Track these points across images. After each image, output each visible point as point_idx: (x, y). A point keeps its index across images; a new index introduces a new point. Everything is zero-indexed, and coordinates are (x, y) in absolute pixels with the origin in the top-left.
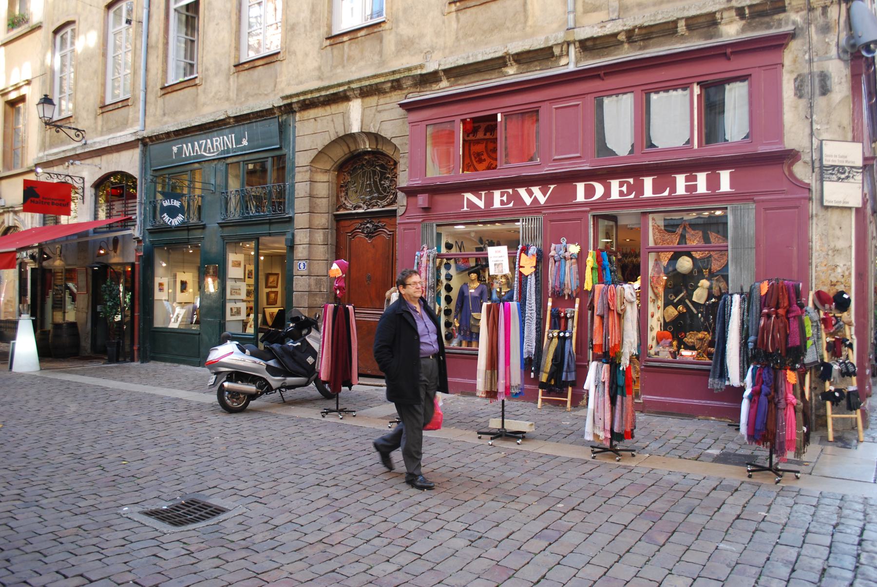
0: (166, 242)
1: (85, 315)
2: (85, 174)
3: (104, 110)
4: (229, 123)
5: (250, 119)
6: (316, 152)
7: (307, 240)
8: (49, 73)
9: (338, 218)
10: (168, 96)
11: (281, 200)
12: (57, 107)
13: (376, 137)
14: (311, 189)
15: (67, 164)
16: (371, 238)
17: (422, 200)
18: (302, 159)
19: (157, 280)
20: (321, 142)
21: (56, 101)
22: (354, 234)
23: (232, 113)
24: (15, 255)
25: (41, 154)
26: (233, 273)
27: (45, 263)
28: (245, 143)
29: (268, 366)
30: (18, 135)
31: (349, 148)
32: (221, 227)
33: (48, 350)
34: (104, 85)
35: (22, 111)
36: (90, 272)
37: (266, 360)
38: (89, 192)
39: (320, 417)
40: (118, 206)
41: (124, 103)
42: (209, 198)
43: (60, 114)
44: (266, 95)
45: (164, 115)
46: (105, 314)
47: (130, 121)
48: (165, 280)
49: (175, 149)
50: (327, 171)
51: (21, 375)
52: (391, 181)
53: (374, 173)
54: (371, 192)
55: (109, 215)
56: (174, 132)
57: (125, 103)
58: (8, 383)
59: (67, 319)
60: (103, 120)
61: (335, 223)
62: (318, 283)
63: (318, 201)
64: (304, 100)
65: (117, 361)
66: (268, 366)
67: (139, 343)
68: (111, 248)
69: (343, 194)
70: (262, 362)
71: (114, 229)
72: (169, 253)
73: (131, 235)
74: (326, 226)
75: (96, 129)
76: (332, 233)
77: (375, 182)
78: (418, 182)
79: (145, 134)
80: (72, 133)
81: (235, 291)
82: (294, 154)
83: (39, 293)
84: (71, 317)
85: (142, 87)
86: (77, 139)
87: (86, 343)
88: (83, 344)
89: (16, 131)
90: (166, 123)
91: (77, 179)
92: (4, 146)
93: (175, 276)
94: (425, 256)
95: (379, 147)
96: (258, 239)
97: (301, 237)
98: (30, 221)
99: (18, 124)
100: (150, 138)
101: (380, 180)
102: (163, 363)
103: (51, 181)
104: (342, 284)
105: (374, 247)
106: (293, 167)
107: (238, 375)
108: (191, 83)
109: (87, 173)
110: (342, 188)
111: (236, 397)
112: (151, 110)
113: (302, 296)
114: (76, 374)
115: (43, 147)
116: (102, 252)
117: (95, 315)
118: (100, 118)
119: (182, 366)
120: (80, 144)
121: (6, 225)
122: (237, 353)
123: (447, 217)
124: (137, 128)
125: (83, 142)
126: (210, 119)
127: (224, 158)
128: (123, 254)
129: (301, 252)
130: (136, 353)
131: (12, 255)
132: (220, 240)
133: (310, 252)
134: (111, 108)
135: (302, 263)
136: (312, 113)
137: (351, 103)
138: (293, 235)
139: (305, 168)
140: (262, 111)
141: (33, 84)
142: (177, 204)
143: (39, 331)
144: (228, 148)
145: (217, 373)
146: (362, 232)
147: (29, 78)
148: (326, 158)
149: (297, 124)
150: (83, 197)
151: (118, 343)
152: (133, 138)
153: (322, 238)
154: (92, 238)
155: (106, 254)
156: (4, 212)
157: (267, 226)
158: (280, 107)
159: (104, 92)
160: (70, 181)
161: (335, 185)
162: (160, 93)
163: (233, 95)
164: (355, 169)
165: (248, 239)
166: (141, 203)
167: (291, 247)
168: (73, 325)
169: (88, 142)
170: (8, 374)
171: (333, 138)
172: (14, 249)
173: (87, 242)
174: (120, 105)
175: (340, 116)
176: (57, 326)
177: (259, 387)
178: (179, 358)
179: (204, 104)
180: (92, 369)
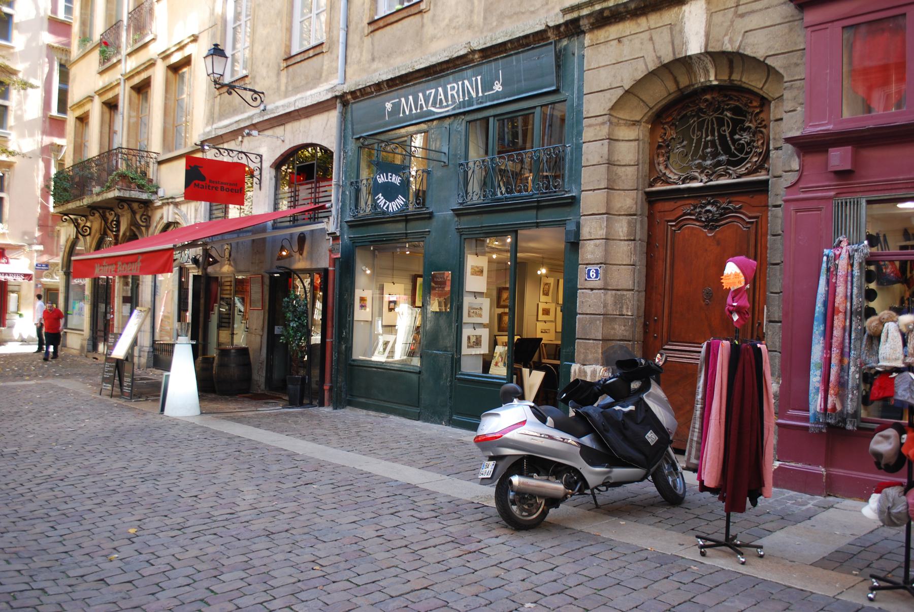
0: (372, 237)
1: (258, 339)
2: (263, 151)
3: (289, 62)
4: (472, 61)
5: (506, 51)
6: (620, 92)
7: (602, 233)
8: (219, 23)
9: (652, 198)
10: (378, 33)
11: (559, 167)
12: (229, 60)
13: (731, 60)
14: (610, 152)
15: (240, 138)
16: (712, 229)
17: (838, 158)
18: (595, 106)
19: (358, 293)
20: (628, 76)
21: (228, 53)
22: (680, 223)
23: (478, 44)
24: (172, 255)
25: (208, 129)
26: (475, 283)
27: (210, 269)
28: (498, 87)
29: (583, 447)
30: (182, 108)
31: (677, 82)
32: (458, 215)
33: (209, 385)
34: (290, 30)
35: (187, 76)
36: (267, 281)
37: (579, 437)
38: (268, 175)
39: (693, 554)
40: (304, 192)
41: (317, 50)
42: (438, 173)
43: (232, 75)
44: (533, 12)
45: (373, 60)
46: (287, 338)
47: (324, 75)
48: (368, 294)
49: (389, 106)
50: (635, 123)
51: (175, 423)
52: (754, 134)
53: (721, 122)
54: (715, 155)
55: (294, 203)
56: (388, 81)
57: (318, 50)
58: (156, 435)
59: (235, 342)
60: (288, 76)
61: (646, 207)
62: (618, 301)
63: (621, 171)
64: (602, 11)
65: (301, 404)
66: (583, 447)
67: (331, 381)
68: (296, 248)
69: (661, 159)
70: (571, 439)
71: (300, 222)
72: (374, 256)
73: (323, 230)
74: (633, 211)
75: (278, 88)
76: (642, 222)
77: (722, 138)
78: (827, 126)
79: (346, 88)
80: (248, 95)
81: (477, 311)
82: (580, 98)
83: (202, 308)
84: (240, 340)
85: (342, 24)
86: (254, 104)
87: (259, 377)
88: (255, 377)
89: (179, 102)
90: (375, 71)
91: (253, 157)
92: (165, 122)
93: (382, 289)
94: (844, 255)
95: (736, 77)
96: (516, 232)
97: (591, 228)
98: (194, 213)
99: (182, 93)
100: (353, 93)
101: (732, 133)
102: (365, 412)
103: (220, 158)
104: (745, 302)
105: (718, 243)
106: (579, 118)
107: (534, 462)
108: (414, 10)
109: (267, 148)
110: (658, 149)
111: (523, 501)
112: (354, 55)
113: (591, 322)
114: (249, 424)
115: (211, 118)
116: (284, 253)
117: (272, 338)
118: (284, 73)
119: (392, 418)
120: (257, 111)
121: (165, 221)
122: (532, 423)
123: (891, 185)
124: (335, 81)
125: (262, 107)
126: (443, 57)
127: (464, 113)
128: (311, 257)
129: (590, 251)
130: (327, 394)
131: (168, 254)
132: (457, 235)
133: (606, 251)
134: (298, 58)
135: (593, 269)
136: (614, 31)
137: (686, 8)
138: (578, 225)
139: (600, 119)
140: (526, 37)
141: (201, 40)
142: (396, 180)
143: (200, 358)
144: (470, 97)
145: (497, 458)
146: (696, 220)
147: (196, 33)
148: (635, 101)
149: (587, 52)
150: (260, 180)
151: (303, 379)
152: (329, 96)
153: (625, 229)
154: (270, 234)
155: (289, 256)
156: (163, 204)
157: (533, 213)
158: (558, 27)
159: (290, 39)
160: (244, 161)
161: (647, 145)
162: (367, 30)
163: (478, 19)
164: (684, 118)
165: (499, 233)
166: (338, 185)
167: (574, 244)
168: (243, 352)
169: (268, 107)
170: (158, 420)
171: (652, 67)
172: (170, 246)
173: (264, 239)
174: (311, 53)
175: (666, 32)
176: (224, 353)
177: (568, 485)
178: (388, 405)
179: (433, 38)
180: (270, 415)
